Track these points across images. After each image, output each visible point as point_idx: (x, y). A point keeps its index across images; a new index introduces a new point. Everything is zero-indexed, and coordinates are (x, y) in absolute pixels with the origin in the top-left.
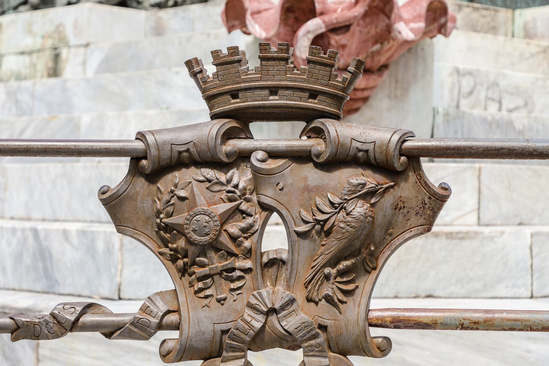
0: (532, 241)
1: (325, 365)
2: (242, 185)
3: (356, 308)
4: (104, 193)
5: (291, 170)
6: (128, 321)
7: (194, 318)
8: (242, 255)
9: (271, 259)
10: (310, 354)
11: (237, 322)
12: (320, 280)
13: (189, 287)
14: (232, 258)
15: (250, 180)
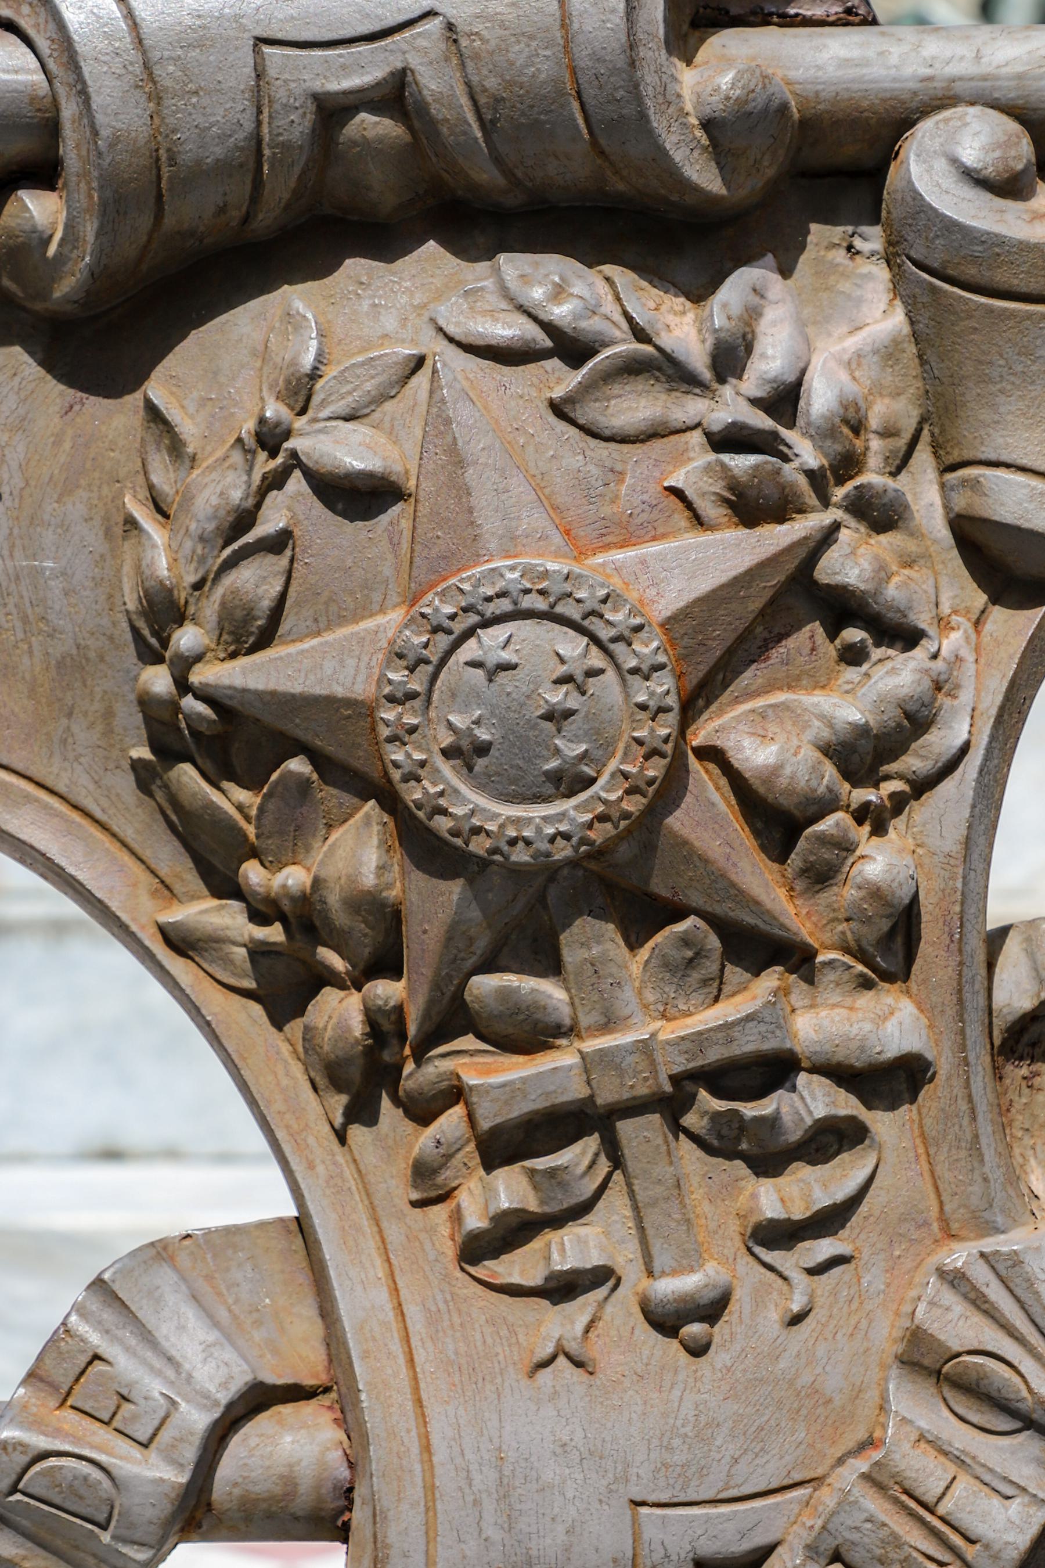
2: (836, 391)
7: (469, 1455)
8: (847, 950)
13: (416, 1204)
14: (757, 974)
15: (889, 353)
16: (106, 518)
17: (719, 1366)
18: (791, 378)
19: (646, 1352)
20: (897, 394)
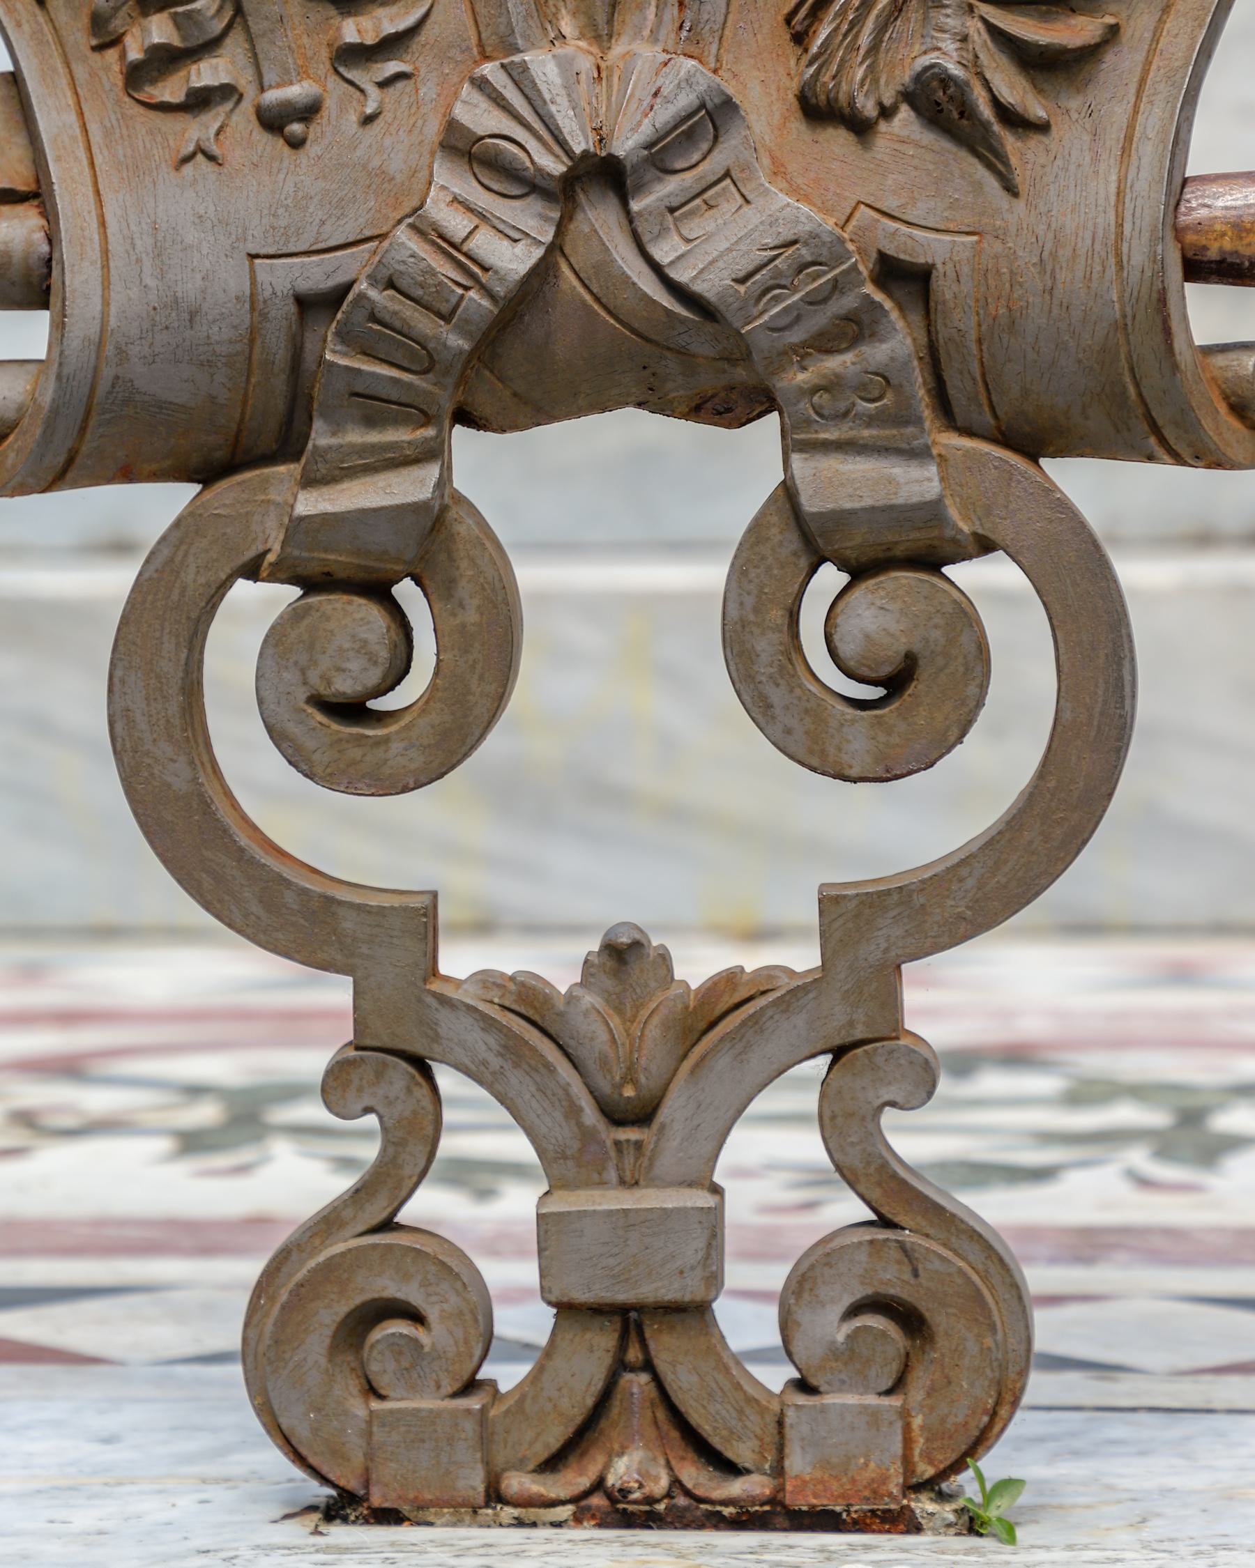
1: (915, 499)
7: (133, 227)
11: (386, 244)
17: (312, 155)
19: (260, 148)
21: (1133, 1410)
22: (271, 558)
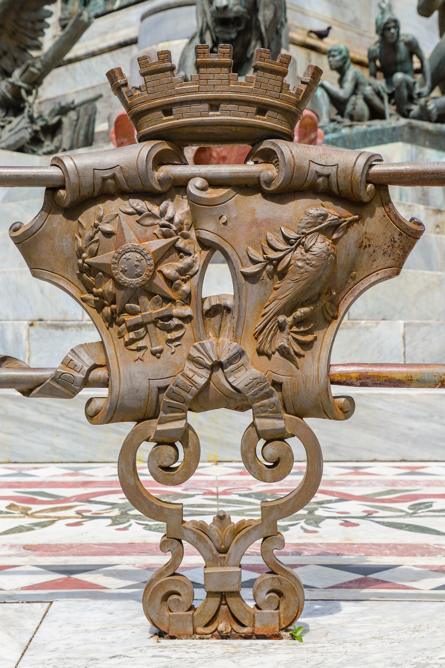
0: (405, 331)
1: (280, 427)
3: (316, 363)
4: (15, 230)
5: (236, 201)
6: (48, 377)
8: (180, 300)
9: (214, 305)
10: (262, 415)
11: (176, 378)
12: (273, 329)
13: (118, 338)
15: (187, 213)
16: (73, 237)
18: (172, 217)
20: (188, 219)
21: (318, 600)
22: (151, 438)
